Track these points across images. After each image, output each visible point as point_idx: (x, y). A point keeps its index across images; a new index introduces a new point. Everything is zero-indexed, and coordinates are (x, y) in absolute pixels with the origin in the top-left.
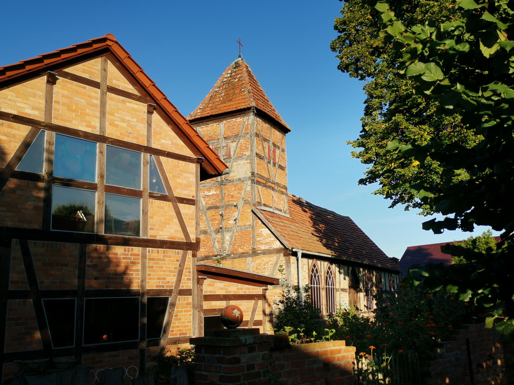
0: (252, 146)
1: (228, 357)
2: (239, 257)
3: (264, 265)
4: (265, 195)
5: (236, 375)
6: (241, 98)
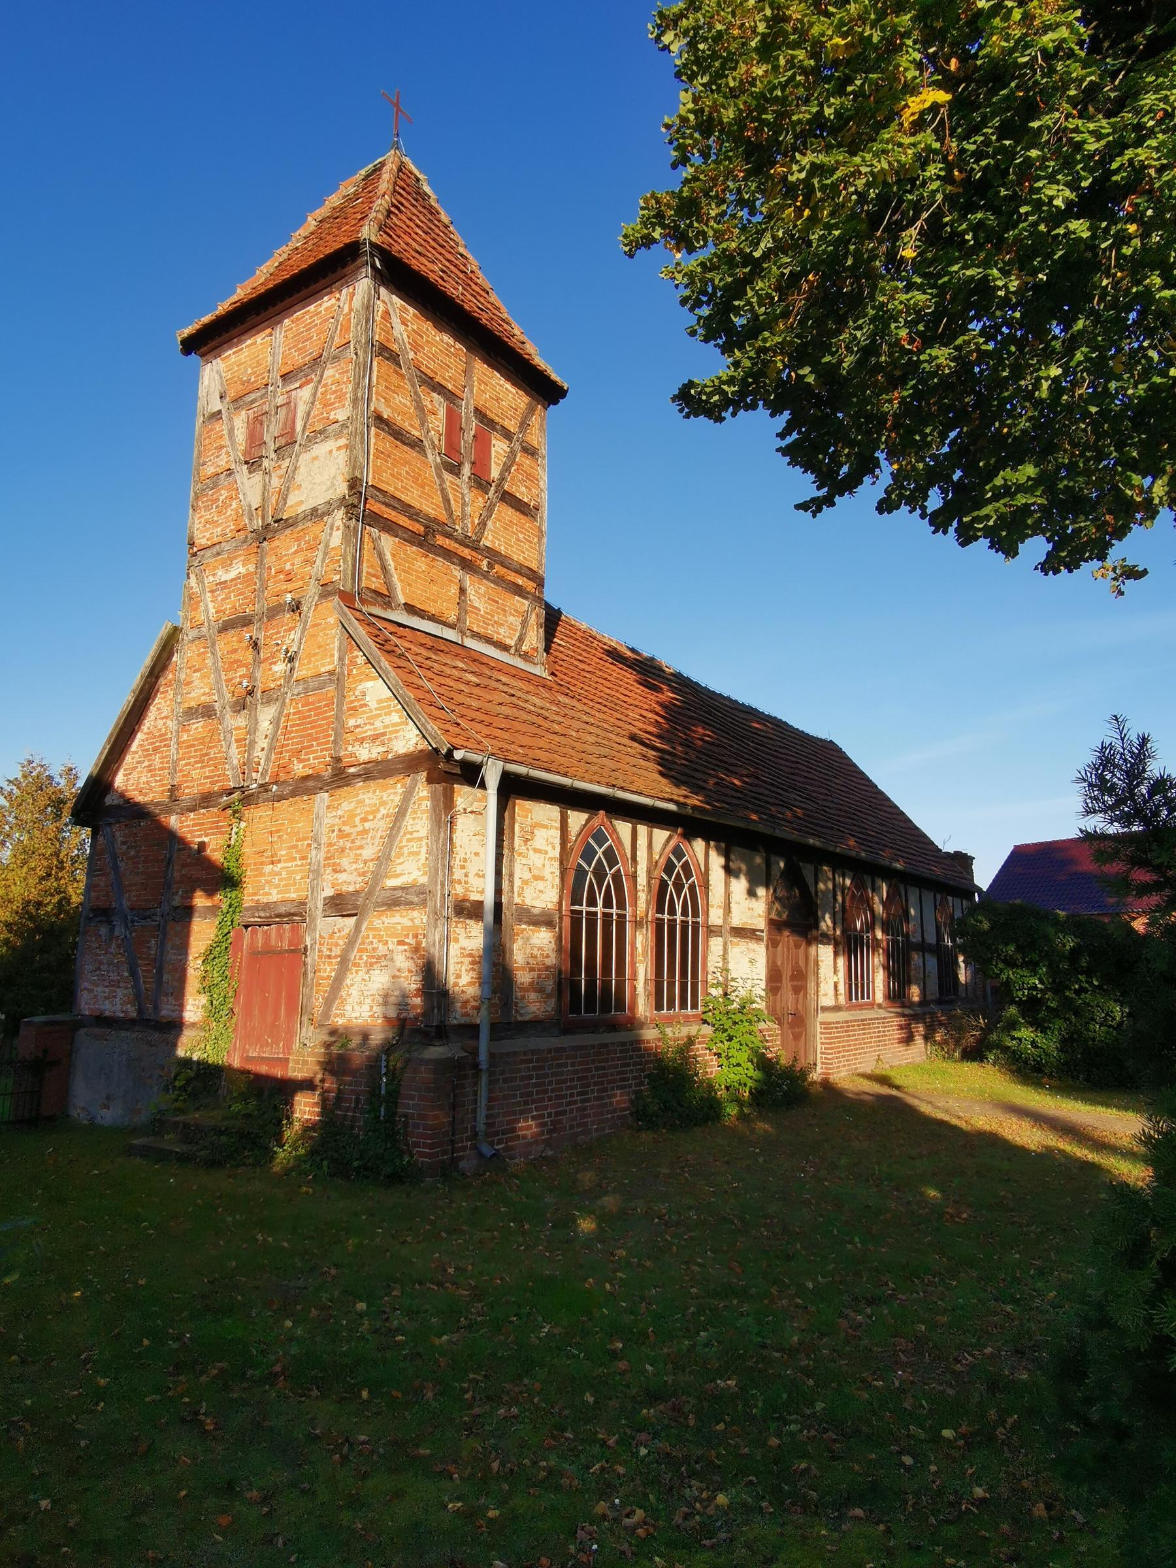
2: (293, 794)
3: (364, 820)
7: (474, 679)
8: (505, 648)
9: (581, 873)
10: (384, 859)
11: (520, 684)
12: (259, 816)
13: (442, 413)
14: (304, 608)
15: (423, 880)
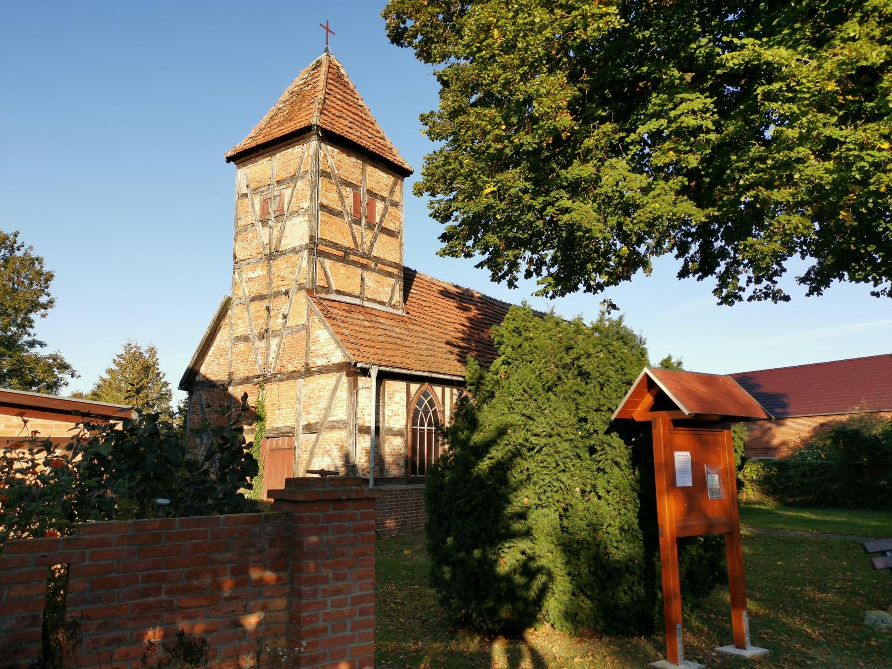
2: (288, 379)
3: (319, 391)
7: (367, 324)
8: (383, 303)
9: (416, 412)
10: (328, 409)
11: (390, 322)
12: (272, 389)
13: (351, 196)
14: (290, 294)
15: (345, 418)
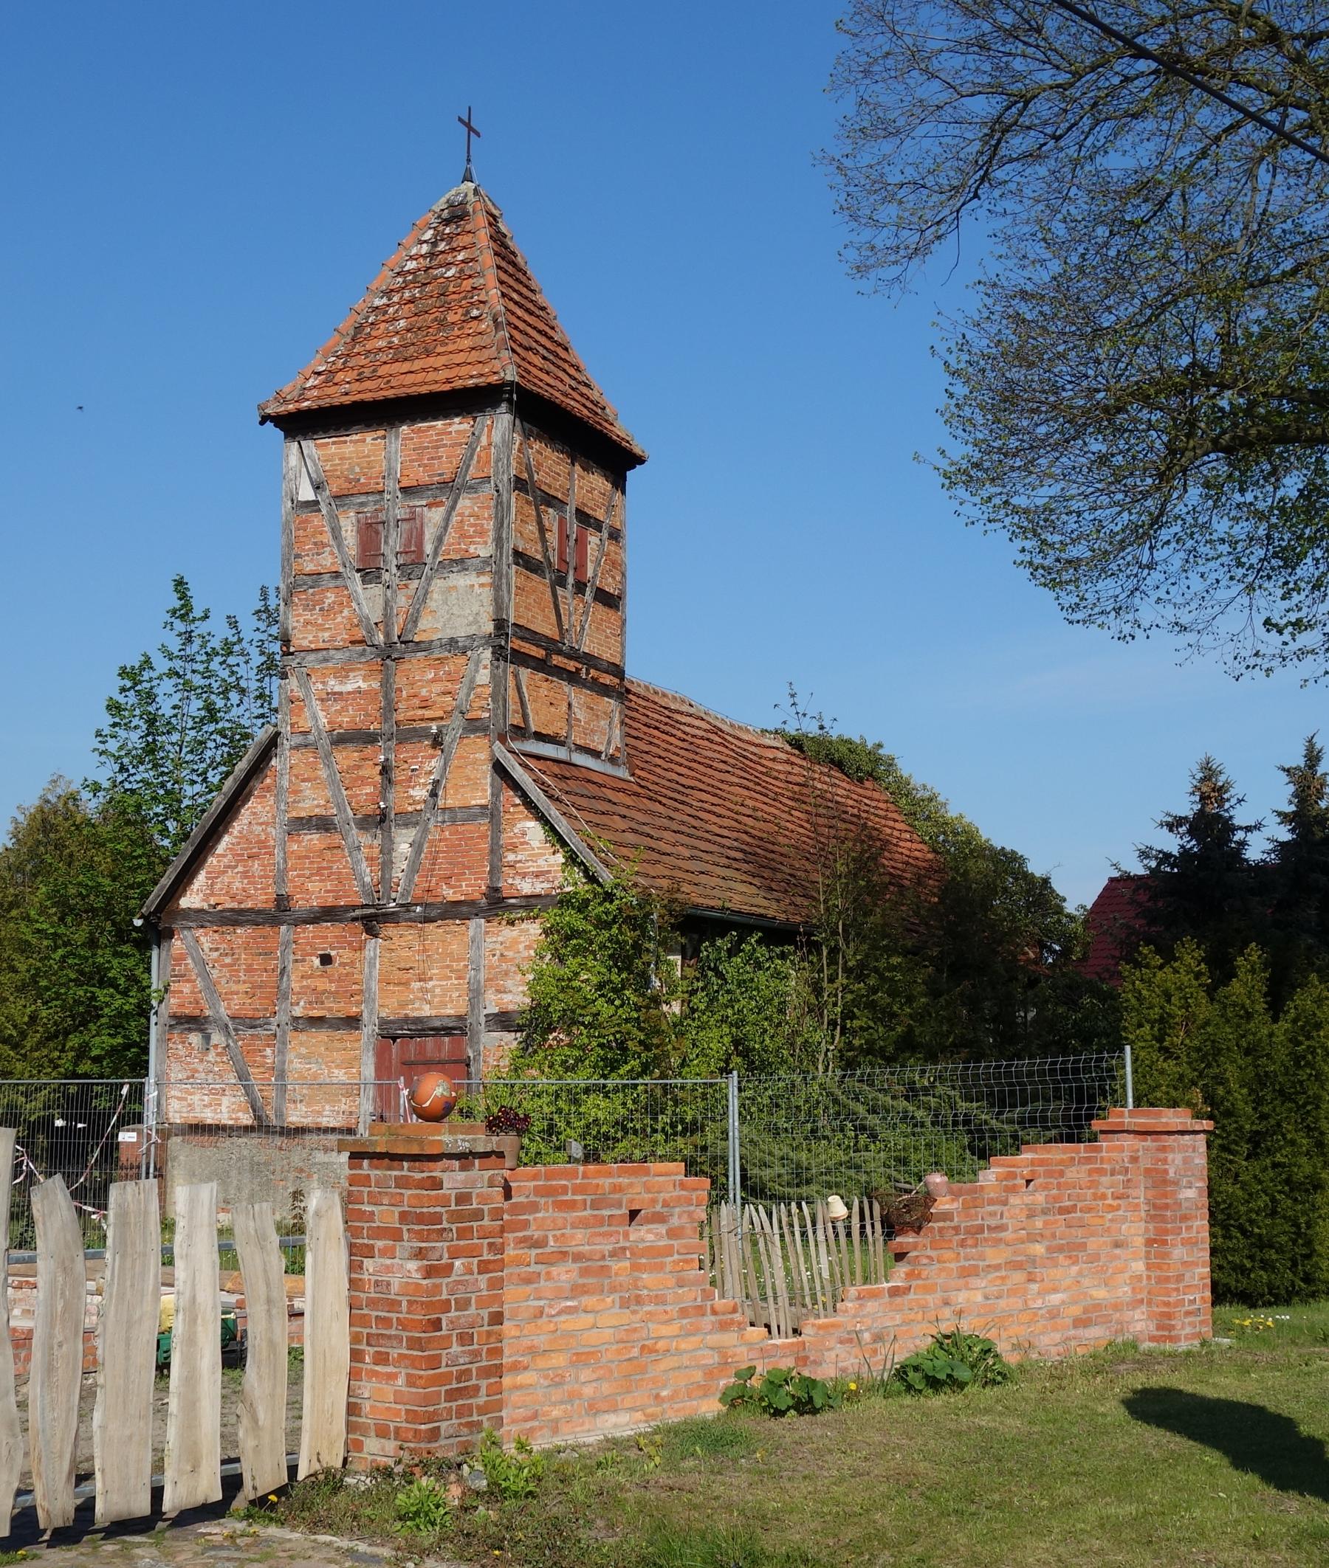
0: (499, 527)
1: (418, 1176)
2: (443, 917)
4: (546, 702)
5: (432, 1210)
6: (467, 343)
